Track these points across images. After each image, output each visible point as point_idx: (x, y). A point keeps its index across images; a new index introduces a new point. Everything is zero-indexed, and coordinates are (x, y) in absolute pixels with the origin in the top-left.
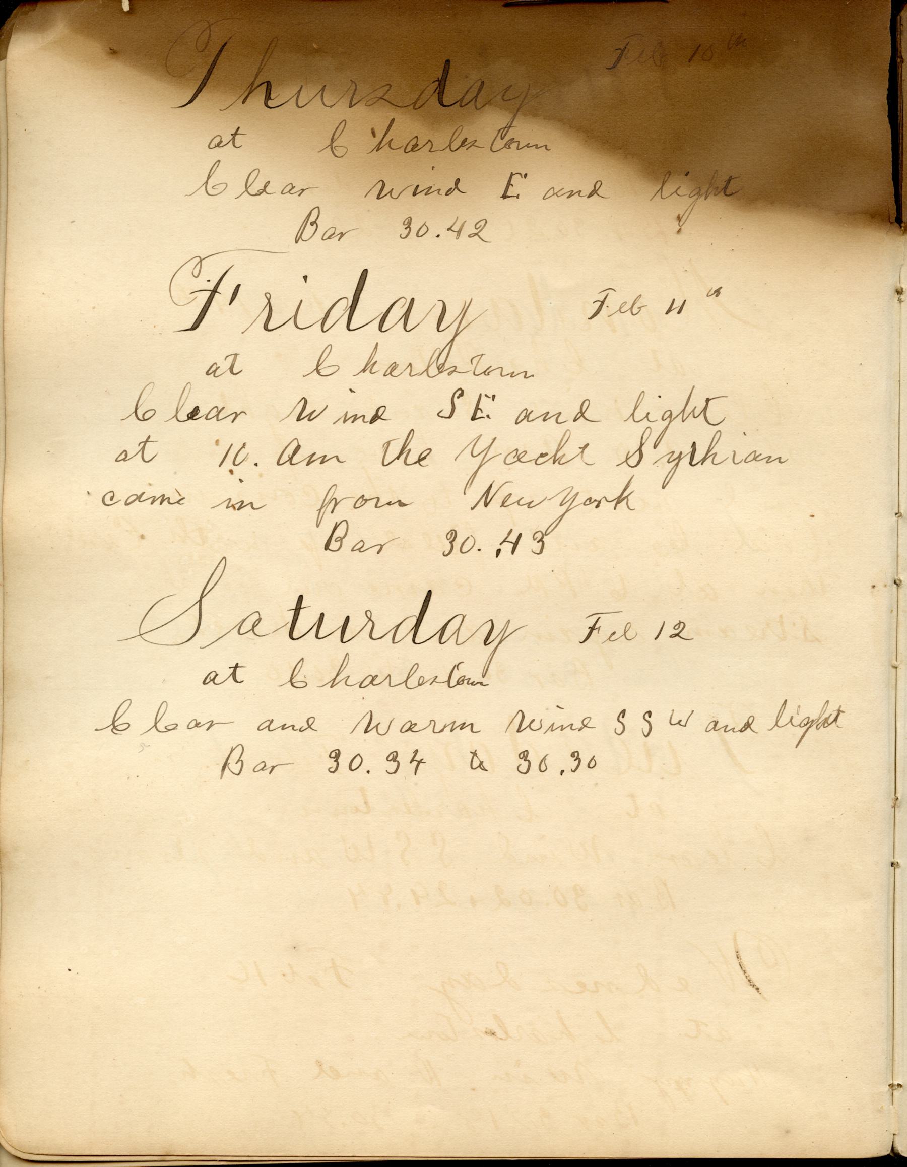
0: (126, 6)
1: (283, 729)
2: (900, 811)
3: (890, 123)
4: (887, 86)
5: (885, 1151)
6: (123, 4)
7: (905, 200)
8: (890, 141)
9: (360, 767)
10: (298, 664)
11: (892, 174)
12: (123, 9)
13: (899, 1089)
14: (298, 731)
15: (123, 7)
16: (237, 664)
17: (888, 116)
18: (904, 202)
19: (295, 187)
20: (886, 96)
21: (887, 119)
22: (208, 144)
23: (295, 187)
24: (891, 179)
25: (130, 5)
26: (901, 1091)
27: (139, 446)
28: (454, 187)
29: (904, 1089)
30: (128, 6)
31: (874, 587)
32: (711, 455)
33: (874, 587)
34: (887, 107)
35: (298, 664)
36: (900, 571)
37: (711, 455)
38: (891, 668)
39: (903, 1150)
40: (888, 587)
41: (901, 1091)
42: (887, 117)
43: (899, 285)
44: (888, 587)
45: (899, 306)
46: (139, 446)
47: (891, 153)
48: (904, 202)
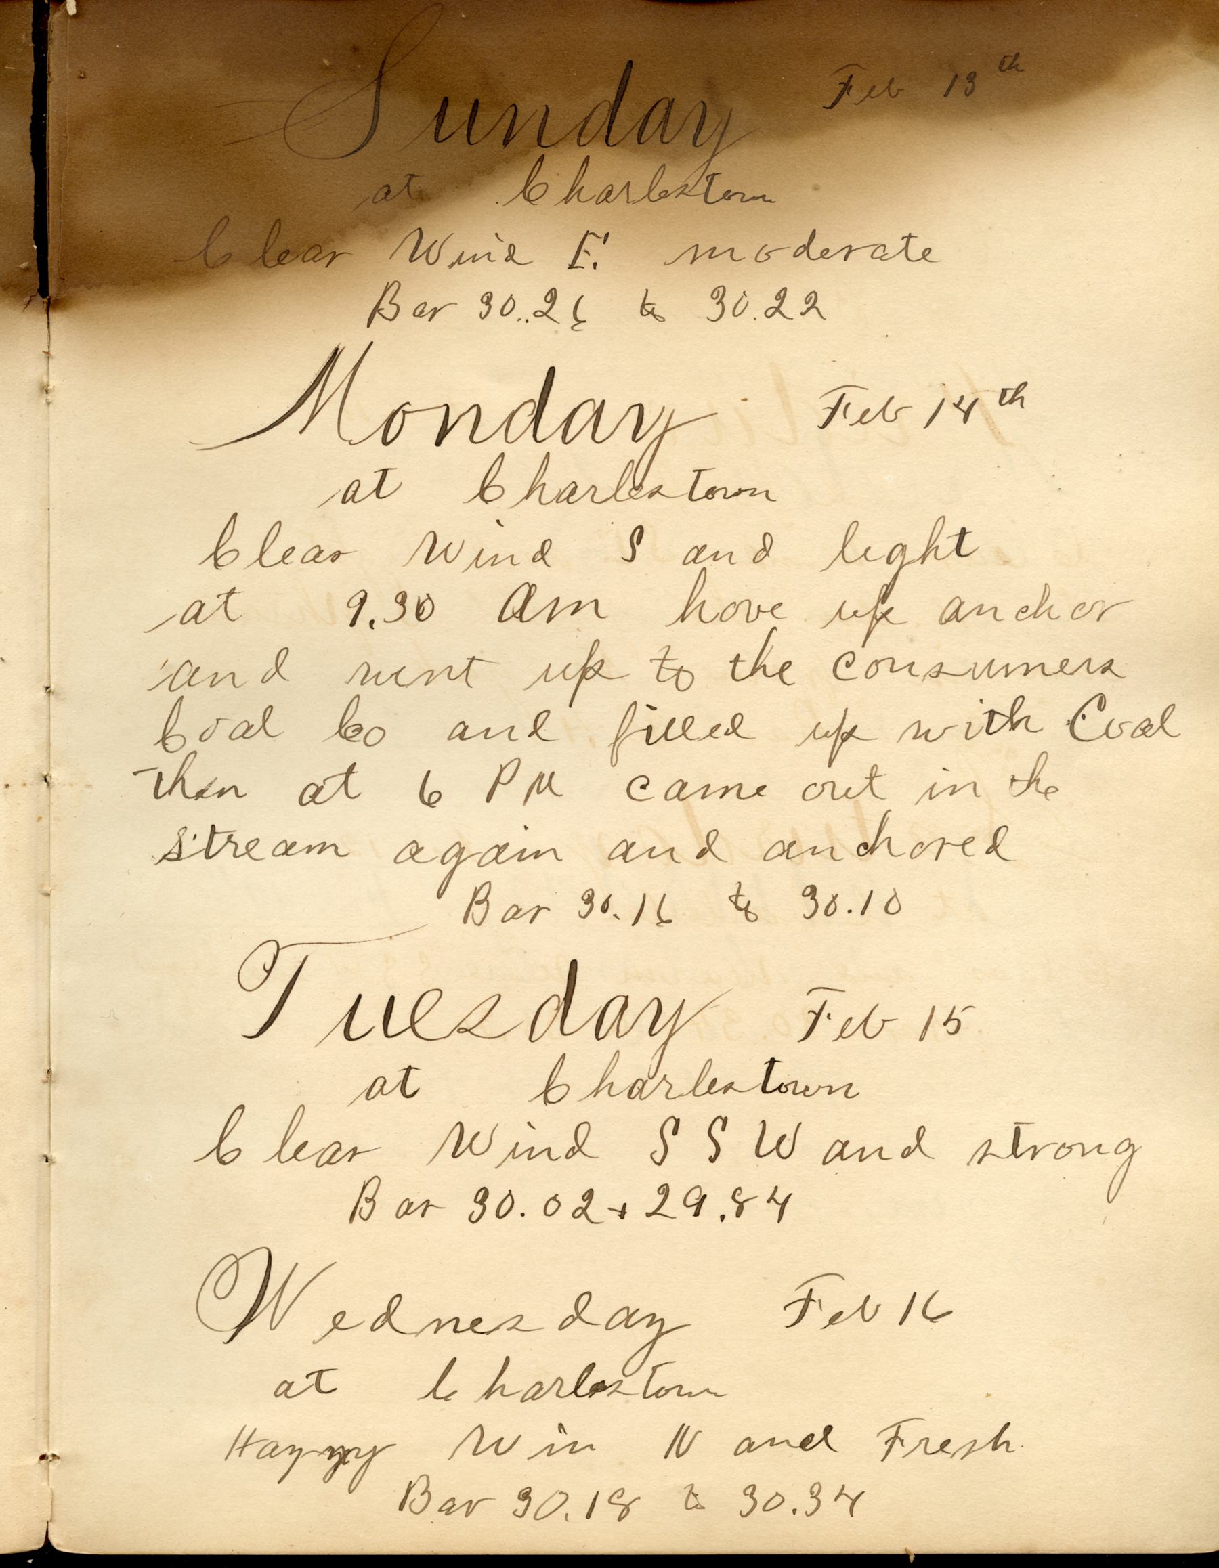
0: (71, 8)
1: (520, 860)
2: (55, 1088)
3: (34, 162)
4: (30, 113)
5: (36, 1544)
6: (67, 5)
7: (52, 267)
8: (32, 187)
9: (767, 1156)
10: (272, 529)
11: (35, 231)
12: (67, 12)
13: (56, 1461)
14: (649, 1080)
15: (68, 9)
16: (733, 1083)
17: (31, 154)
18: (52, 269)
19: (423, 848)
20: (29, 127)
21: (29, 158)
22: (289, 653)
23: (423, 848)
24: (32, 238)
25: (77, 6)
26: (58, 1464)
27: (561, 1432)
28: (913, 1143)
29: (62, 1461)
30: (75, 7)
31: (7, 786)
32: (932, 550)
33: (7, 786)
34: (29, 141)
35: (272, 529)
36: (52, 765)
37: (932, 550)
38: (41, 896)
39: (61, 1543)
40: (29, 787)
41: (58, 1464)
42: (29, 154)
43: (45, 380)
44: (29, 787)
45: (44, 366)
46: (561, 1432)
47: (32, 201)
48: (52, 269)
